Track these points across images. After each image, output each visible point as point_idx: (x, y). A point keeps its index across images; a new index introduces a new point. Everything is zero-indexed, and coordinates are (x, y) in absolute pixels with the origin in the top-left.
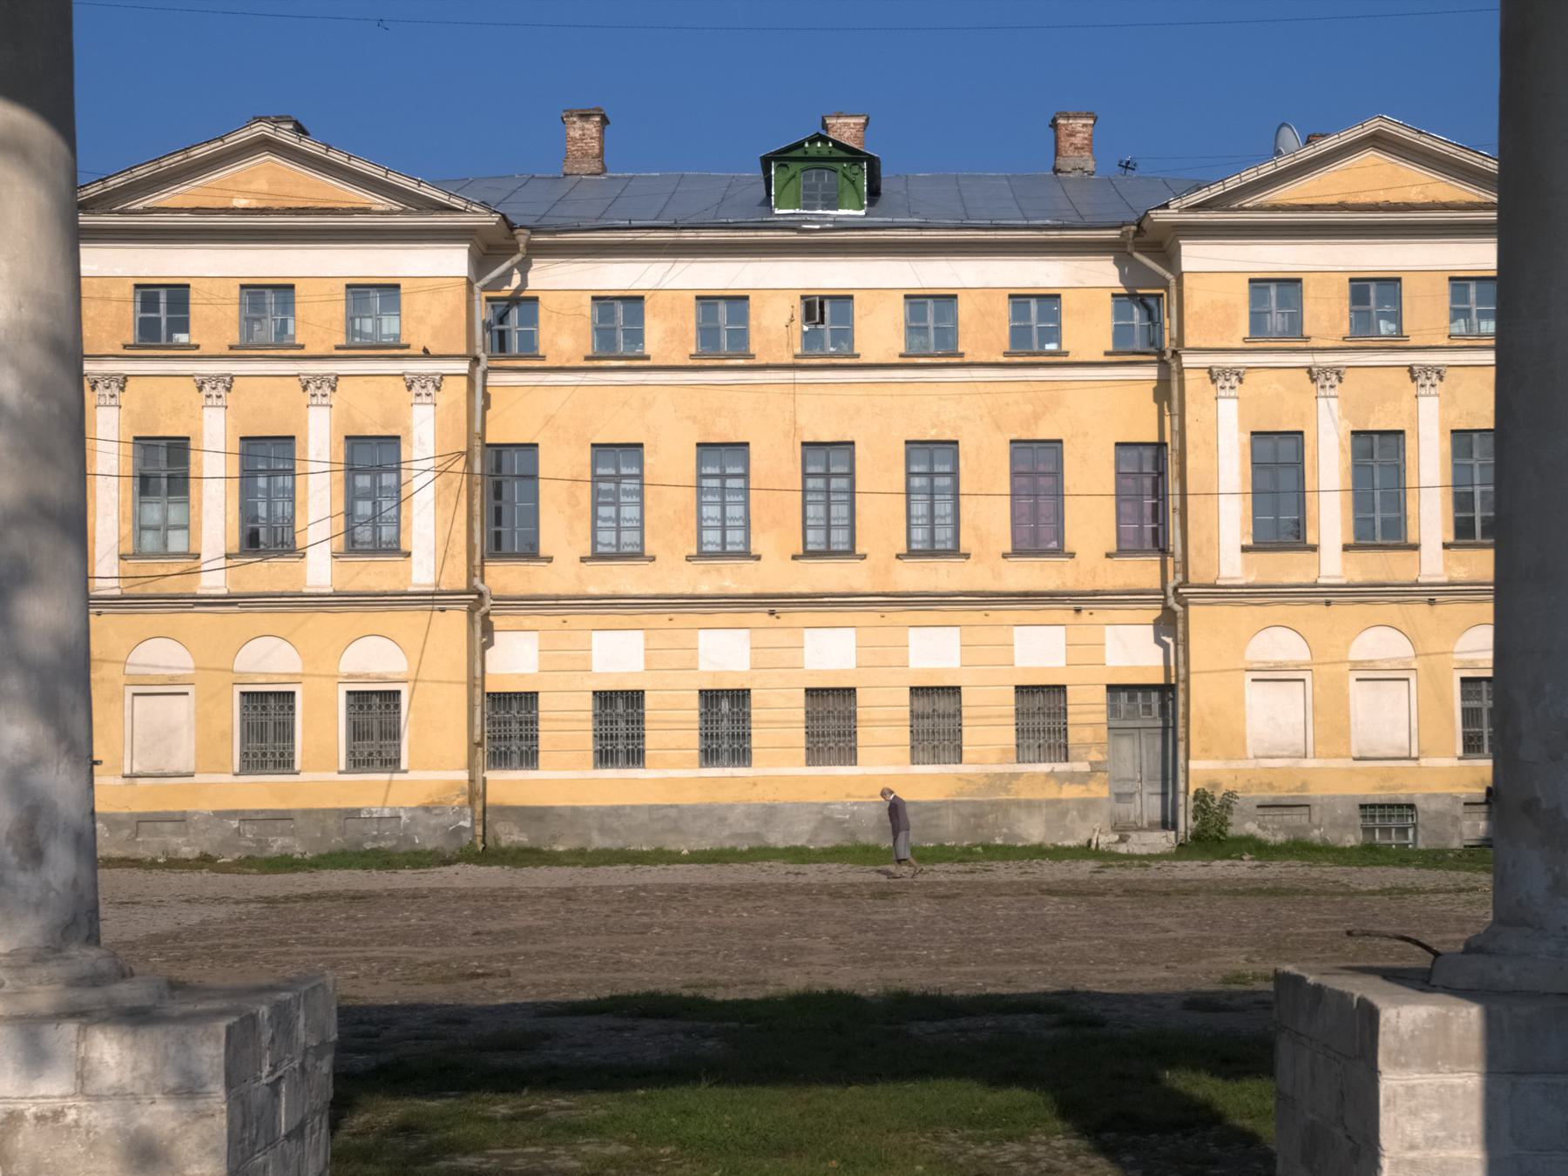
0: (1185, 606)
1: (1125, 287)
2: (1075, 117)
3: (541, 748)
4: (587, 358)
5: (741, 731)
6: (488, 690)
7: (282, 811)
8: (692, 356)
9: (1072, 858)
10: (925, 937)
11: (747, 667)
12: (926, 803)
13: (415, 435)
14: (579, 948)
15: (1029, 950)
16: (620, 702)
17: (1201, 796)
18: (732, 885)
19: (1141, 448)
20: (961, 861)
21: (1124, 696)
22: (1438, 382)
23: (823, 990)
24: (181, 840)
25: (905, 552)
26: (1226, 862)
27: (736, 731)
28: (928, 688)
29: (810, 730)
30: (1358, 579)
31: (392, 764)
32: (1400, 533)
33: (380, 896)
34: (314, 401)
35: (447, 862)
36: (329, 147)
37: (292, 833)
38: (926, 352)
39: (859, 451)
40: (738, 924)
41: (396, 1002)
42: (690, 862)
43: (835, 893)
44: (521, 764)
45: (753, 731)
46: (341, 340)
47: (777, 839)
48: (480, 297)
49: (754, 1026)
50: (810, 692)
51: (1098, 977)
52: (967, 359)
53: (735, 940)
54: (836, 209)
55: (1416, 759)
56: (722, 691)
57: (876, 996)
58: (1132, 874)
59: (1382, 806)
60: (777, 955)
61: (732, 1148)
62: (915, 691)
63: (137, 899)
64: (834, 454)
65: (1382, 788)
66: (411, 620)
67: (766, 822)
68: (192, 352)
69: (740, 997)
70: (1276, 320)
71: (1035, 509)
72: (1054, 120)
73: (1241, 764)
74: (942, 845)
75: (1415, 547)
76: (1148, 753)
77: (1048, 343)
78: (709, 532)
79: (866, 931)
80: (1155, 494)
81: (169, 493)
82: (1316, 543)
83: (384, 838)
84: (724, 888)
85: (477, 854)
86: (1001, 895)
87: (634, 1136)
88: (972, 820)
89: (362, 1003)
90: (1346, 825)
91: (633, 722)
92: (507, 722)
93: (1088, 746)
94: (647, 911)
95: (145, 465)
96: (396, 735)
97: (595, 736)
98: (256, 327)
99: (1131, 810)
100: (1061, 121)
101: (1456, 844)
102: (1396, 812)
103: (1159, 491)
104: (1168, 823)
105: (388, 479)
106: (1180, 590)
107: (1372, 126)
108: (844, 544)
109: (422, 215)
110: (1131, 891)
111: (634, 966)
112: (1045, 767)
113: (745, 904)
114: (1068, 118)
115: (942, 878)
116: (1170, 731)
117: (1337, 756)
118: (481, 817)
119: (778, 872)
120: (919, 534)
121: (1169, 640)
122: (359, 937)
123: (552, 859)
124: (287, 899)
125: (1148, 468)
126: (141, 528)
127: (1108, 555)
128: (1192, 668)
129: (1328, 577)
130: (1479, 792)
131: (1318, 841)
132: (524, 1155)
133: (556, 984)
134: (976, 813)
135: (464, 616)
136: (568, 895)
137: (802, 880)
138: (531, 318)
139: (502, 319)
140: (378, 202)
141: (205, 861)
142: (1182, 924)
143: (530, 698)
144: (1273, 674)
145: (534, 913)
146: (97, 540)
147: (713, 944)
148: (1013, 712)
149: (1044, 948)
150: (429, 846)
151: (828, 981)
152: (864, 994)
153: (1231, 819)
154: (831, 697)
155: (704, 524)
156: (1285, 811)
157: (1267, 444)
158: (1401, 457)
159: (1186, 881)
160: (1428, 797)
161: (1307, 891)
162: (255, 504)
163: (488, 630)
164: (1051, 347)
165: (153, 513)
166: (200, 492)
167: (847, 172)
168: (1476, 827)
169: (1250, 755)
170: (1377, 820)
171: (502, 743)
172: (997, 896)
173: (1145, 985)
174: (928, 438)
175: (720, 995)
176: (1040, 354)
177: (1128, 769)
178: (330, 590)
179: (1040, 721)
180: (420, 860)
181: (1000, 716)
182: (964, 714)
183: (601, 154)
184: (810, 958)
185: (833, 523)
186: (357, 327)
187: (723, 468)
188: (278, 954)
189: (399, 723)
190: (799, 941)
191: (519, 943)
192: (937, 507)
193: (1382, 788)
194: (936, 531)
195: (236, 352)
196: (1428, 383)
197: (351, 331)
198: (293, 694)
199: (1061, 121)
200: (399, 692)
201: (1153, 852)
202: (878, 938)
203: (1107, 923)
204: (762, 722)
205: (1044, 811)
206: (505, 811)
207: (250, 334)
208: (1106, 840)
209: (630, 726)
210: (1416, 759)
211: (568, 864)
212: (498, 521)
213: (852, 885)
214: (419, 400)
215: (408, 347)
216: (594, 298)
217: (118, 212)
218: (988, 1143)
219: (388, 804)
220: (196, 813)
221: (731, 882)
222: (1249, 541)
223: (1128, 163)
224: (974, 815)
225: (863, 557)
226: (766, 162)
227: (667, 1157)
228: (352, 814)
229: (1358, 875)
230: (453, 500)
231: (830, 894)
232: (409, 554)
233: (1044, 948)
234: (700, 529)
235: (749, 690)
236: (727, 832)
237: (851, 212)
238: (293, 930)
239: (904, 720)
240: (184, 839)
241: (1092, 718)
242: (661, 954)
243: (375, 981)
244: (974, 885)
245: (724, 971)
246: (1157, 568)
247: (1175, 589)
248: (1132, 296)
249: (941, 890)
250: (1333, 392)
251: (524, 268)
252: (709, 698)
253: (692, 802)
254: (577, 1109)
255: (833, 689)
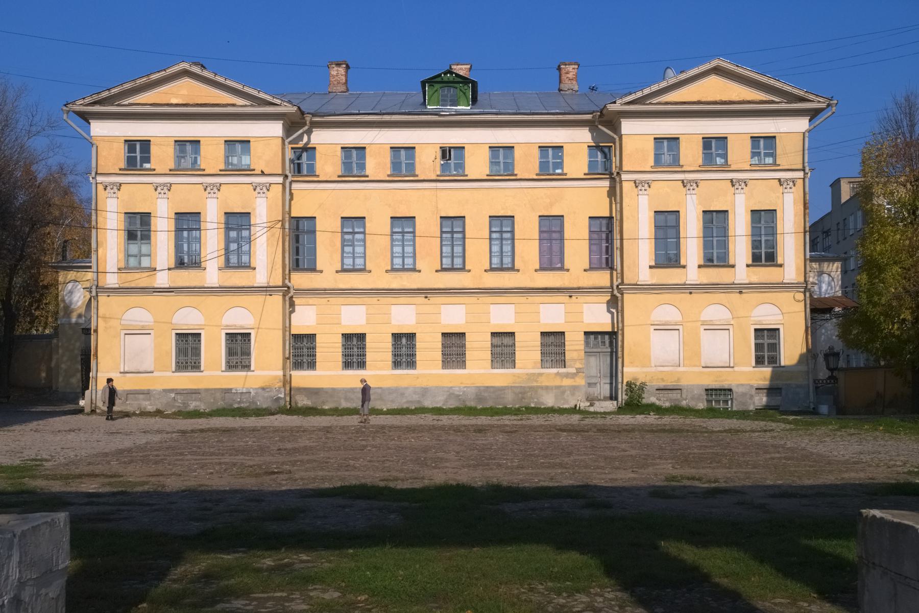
0: (622, 294)
1: (594, 143)
2: (569, 65)
3: (317, 360)
4: (339, 176)
5: (411, 353)
6: (292, 333)
7: (195, 389)
8: (388, 176)
9: (568, 413)
10: (503, 453)
11: (414, 322)
12: (498, 387)
13: (257, 211)
14: (329, 458)
15: (558, 461)
16: (355, 339)
17: (629, 384)
18: (407, 425)
19: (601, 219)
20: (515, 415)
21: (592, 337)
22: (744, 187)
23: (454, 483)
24: (147, 403)
25: (489, 268)
26: (642, 416)
27: (409, 352)
28: (499, 333)
29: (444, 352)
30: (705, 282)
31: (247, 367)
32: (725, 259)
33: (237, 430)
34: (210, 195)
35: (273, 414)
36: (216, 74)
37: (200, 400)
38: (499, 174)
39: (467, 221)
40: (409, 446)
41: (228, 488)
42: (387, 414)
43: (457, 430)
44: (308, 368)
45: (417, 353)
46: (223, 167)
47: (428, 404)
48: (288, 147)
49: (418, 505)
50: (444, 334)
51: (598, 476)
52: (518, 177)
53: (408, 454)
54: (457, 106)
55: (733, 367)
56: (403, 334)
57: (482, 487)
58: (599, 421)
59: (716, 390)
60: (429, 463)
61: (403, 596)
62: (494, 334)
63: (120, 431)
64: (455, 222)
65: (716, 381)
66: (258, 299)
67: (423, 395)
68: (152, 172)
69: (410, 487)
70: (666, 158)
71: (550, 248)
72: (559, 66)
73: (648, 369)
74: (506, 407)
75: (733, 266)
76: (603, 364)
77: (557, 169)
78: (397, 259)
79: (474, 450)
80: (607, 240)
81: (142, 239)
82: (685, 264)
83: (243, 402)
84: (403, 427)
85: (287, 410)
86: (538, 431)
87: (343, 584)
88: (520, 395)
89: (210, 489)
90: (699, 399)
91: (360, 348)
92: (302, 348)
93: (575, 360)
94: (365, 438)
95: (130, 226)
96: (248, 354)
97: (343, 355)
98: (183, 160)
99: (595, 391)
100: (562, 66)
101: (752, 408)
102: (723, 392)
103: (609, 239)
104: (613, 397)
105: (245, 233)
106: (620, 287)
107: (715, 63)
108: (460, 265)
109: (263, 107)
110: (602, 430)
111: (356, 468)
112: (554, 371)
113: (413, 435)
114: (566, 65)
115: (507, 422)
116: (614, 353)
117: (695, 366)
118: (289, 392)
119: (429, 419)
120: (496, 260)
121: (614, 311)
122: (221, 451)
123: (323, 413)
124: (192, 431)
125: (604, 229)
126: (128, 256)
127: (585, 270)
128: (625, 324)
129: (691, 280)
130: (766, 383)
131: (685, 407)
132: (273, 598)
133: (314, 478)
134: (522, 392)
135: (281, 298)
136: (327, 430)
137: (440, 423)
138: (312, 158)
139: (299, 158)
140: (240, 101)
141: (158, 413)
142: (632, 447)
143: (312, 337)
144: (664, 327)
145: (309, 439)
146: (107, 261)
147: (396, 456)
148: (540, 345)
149: (566, 459)
150: (264, 406)
151: (456, 477)
152: (476, 485)
153: (643, 396)
154: (454, 337)
155: (394, 255)
156: (669, 392)
157: (662, 217)
158: (727, 223)
159: (626, 425)
160: (738, 386)
161: (688, 431)
162: (183, 245)
163: (292, 305)
164: (558, 171)
165: (134, 248)
166: (156, 238)
167: (462, 89)
168: (761, 400)
169: (653, 365)
170: (714, 396)
171: (299, 358)
172: (535, 432)
173: (625, 482)
174: (500, 214)
175: (400, 485)
176: (554, 175)
177: (594, 371)
178: (217, 285)
179: (553, 349)
180: (260, 412)
181: (533, 346)
182: (516, 345)
183: (346, 83)
184: (448, 464)
185: (455, 255)
186: (230, 161)
187: (403, 228)
188: (177, 460)
189: (250, 348)
190: (440, 454)
191: (299, 455)
192: (504, 247)
193: (716, 381)
194: (504, 259)
195: (173, 172)
196: (740, 187)
197: (227, 162)
198: (200, 334)
199: (562, 66)
200: (250, 334)
201: (607, 411)
202: (480, 453)
203: (593, 446)
204: (421, 349)
205: (554, 391)
206: (301, 390)
207: (179, 164)
208: (584, 405)
209: (359, 350)
210: (733, 367)
211: (329, 415)
212: (297, 254)
213: (465, 426)
214: (259, 195)
215: (254, 170)
216: (342, 148)
217: (116, 105)
218: (565, 594)
219: (246, 386)
220: (154, 390)
221: (406, 424)
222: (653, 264)
223: (594, 87)
224: (521, 393)
225: (469, 271)
226: (423, 84)
227: (362, 603)
228: (228, 391)
229: (710, 423)
230: (275, 243)
231: (454, 430)
232: (255, 269)
233: (566, 459)
234: (392, 257)
235: (415, 334)
236: (404, 400)
237: (464, 107)
238: (189, 447)
239: (488, 348)
240: (149, 402)
241: (577, 347)
242: (370, 461)
243: (220, 476)
244: (524, 426)
245: (401, 471)
246: (608, 276)
247: (618, 286)
248: (597, 147)
249: (508, 428)
250: (694, 192)
251: (309, 132)
252: (397, 337)
253: (388, 386)
254: (312, 562)
255: (455, 333)
